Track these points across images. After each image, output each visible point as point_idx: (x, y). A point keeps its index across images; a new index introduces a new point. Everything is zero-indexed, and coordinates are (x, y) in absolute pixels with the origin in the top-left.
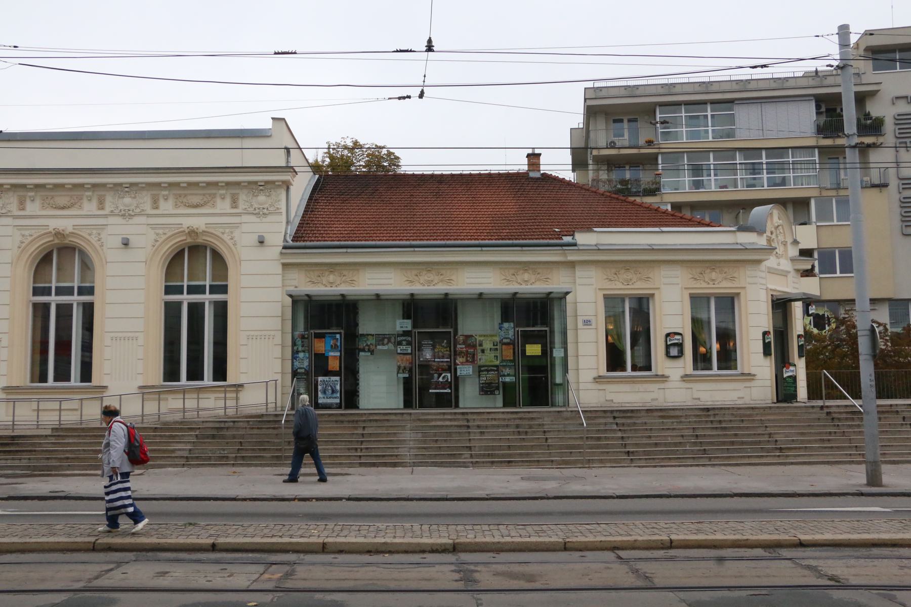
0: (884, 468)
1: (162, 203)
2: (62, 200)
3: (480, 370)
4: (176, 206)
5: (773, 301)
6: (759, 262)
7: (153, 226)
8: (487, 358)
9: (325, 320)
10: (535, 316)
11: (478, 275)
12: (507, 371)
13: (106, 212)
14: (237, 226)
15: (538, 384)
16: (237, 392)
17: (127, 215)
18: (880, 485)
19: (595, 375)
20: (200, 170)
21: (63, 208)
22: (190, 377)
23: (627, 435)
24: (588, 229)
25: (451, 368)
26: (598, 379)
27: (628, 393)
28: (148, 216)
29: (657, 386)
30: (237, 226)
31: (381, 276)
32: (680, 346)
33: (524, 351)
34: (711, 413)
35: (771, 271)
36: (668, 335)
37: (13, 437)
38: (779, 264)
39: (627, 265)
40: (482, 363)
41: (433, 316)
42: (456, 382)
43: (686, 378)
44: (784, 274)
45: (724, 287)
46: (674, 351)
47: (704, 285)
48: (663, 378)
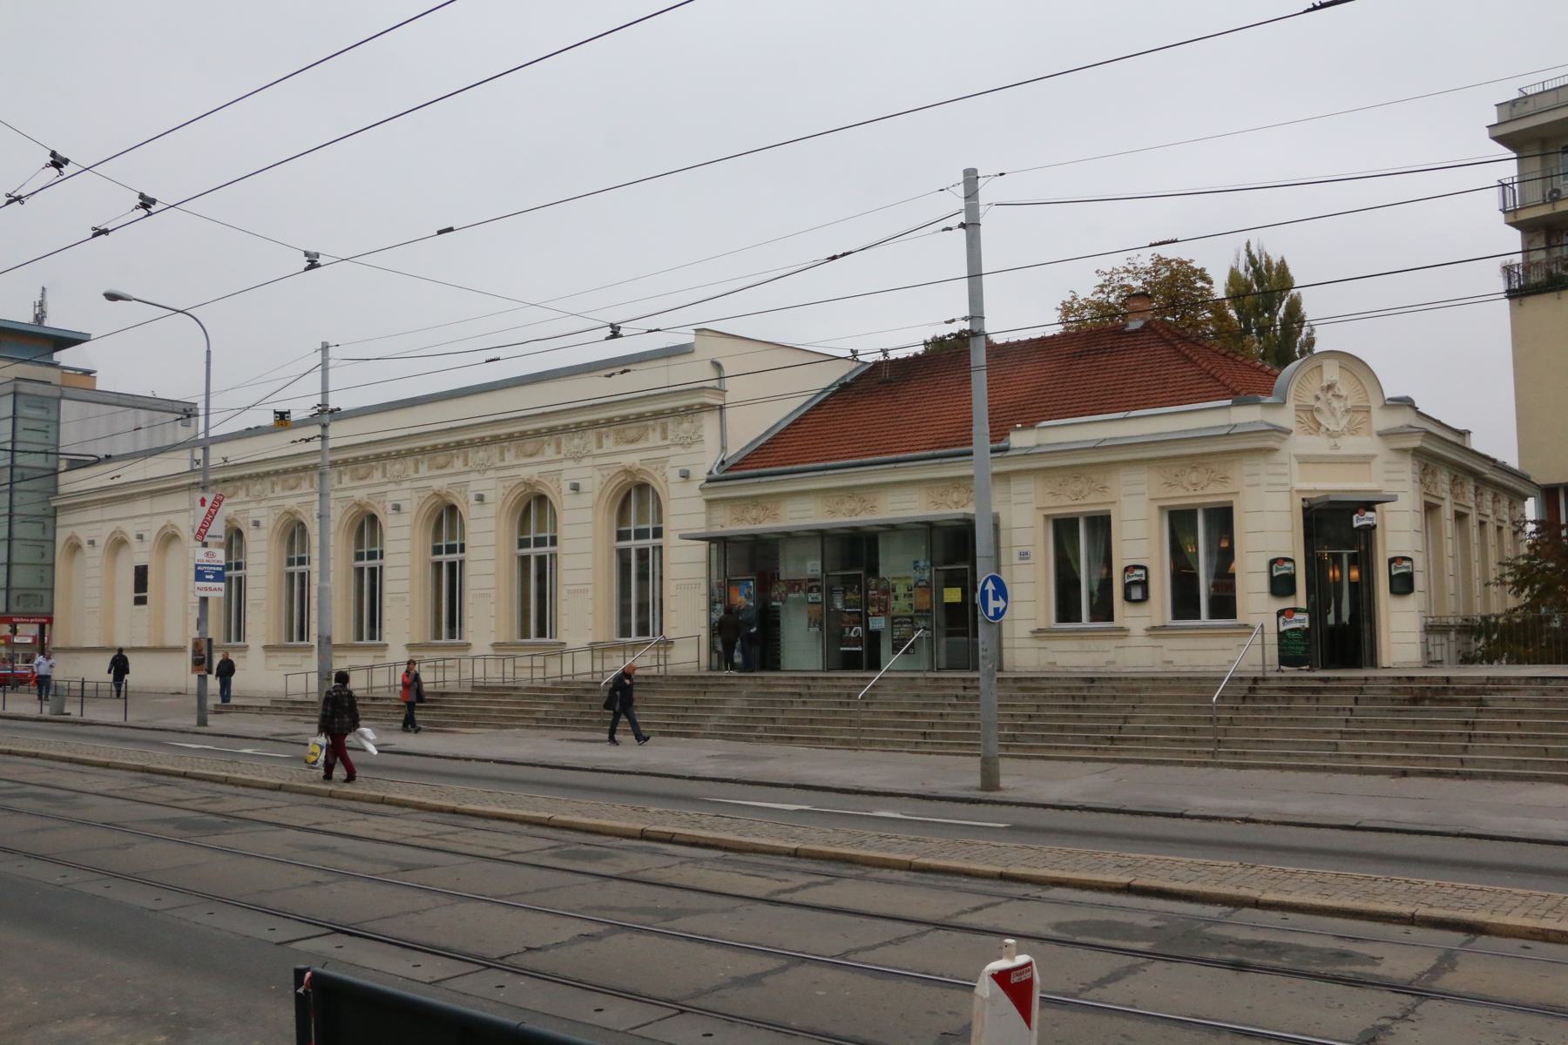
0: (1005, 765)
1: (507, 454)
2: (631, 433)
3: (894, 621)
4: (617, 443)
5: (1305, 510)
6: (1272, 450)
7: (600, 467)
8: (900, 606)
9: (748, 560)
10: (955, 545)
11: (902, 499)
12: (922, 623)
13: (667, 442)
14: (665, 460)
15: (962, 626)
16: (665, 649)
17: (577, 458)
18: (998, 789)
19: (1149, 625)
20: (637, 398)
21: (531, 456)
22: (1095, 617)
23: (1089, 715)
24: (1029, 425)
25: (862, 619)
26: (1039, 633)
27: (1079, 654)
28: (594, 456)
29: (1115, 643)
30: (665, 460)
31: (804, 508)
32: (1144, 585)
33: (964, 593)
34: (1096, 684)
35: (1304, 460)
36: (1273, 562)
37: (442, 694)
38: (1336, 447)
39: (1076, 471)
40: (894, 613)
41: (856, 550)
42: (874, 638)
43: (1154, 631)
44: (1366, 460)
45: (1213, 494)
46: (1137, 593)
47: (1182, 492)
48: (1123, 631)
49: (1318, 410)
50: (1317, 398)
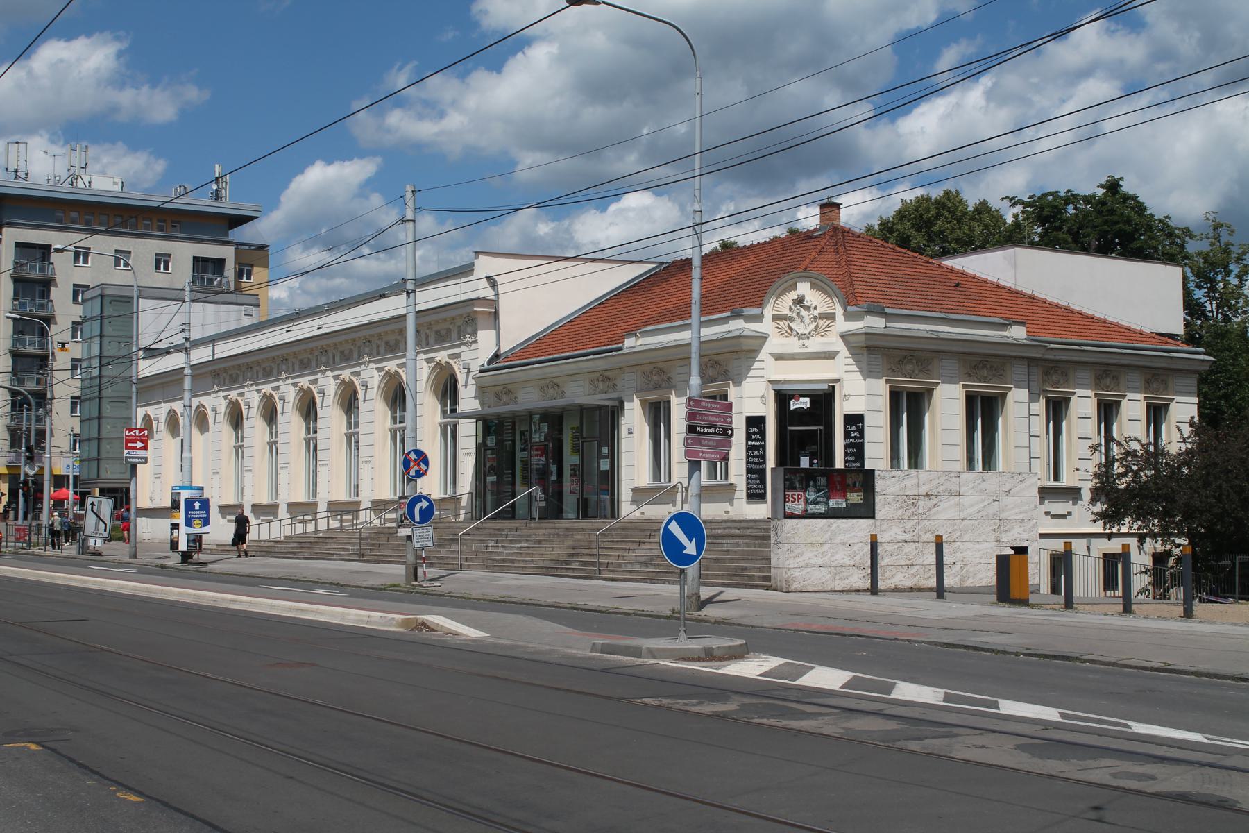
24: (633, 332)
35: (779, 357)
44: (830, 356)
49: (791, 319)
50: (791, 309)
